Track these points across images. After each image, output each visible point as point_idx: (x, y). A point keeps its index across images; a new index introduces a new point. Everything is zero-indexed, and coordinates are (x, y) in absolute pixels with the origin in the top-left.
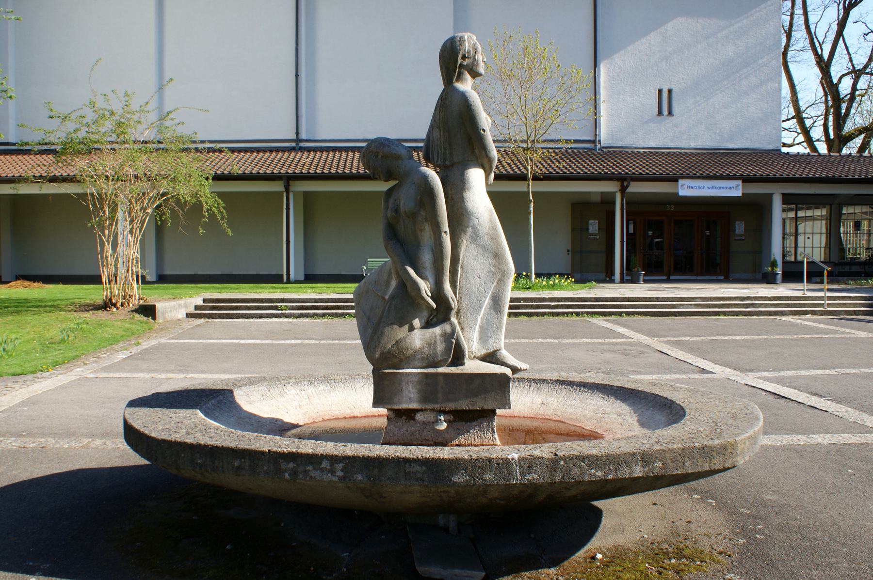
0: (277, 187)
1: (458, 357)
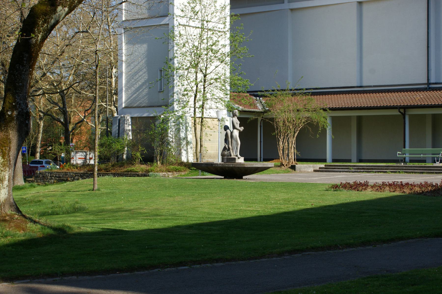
0: (396, 112)
1: (231, 156)
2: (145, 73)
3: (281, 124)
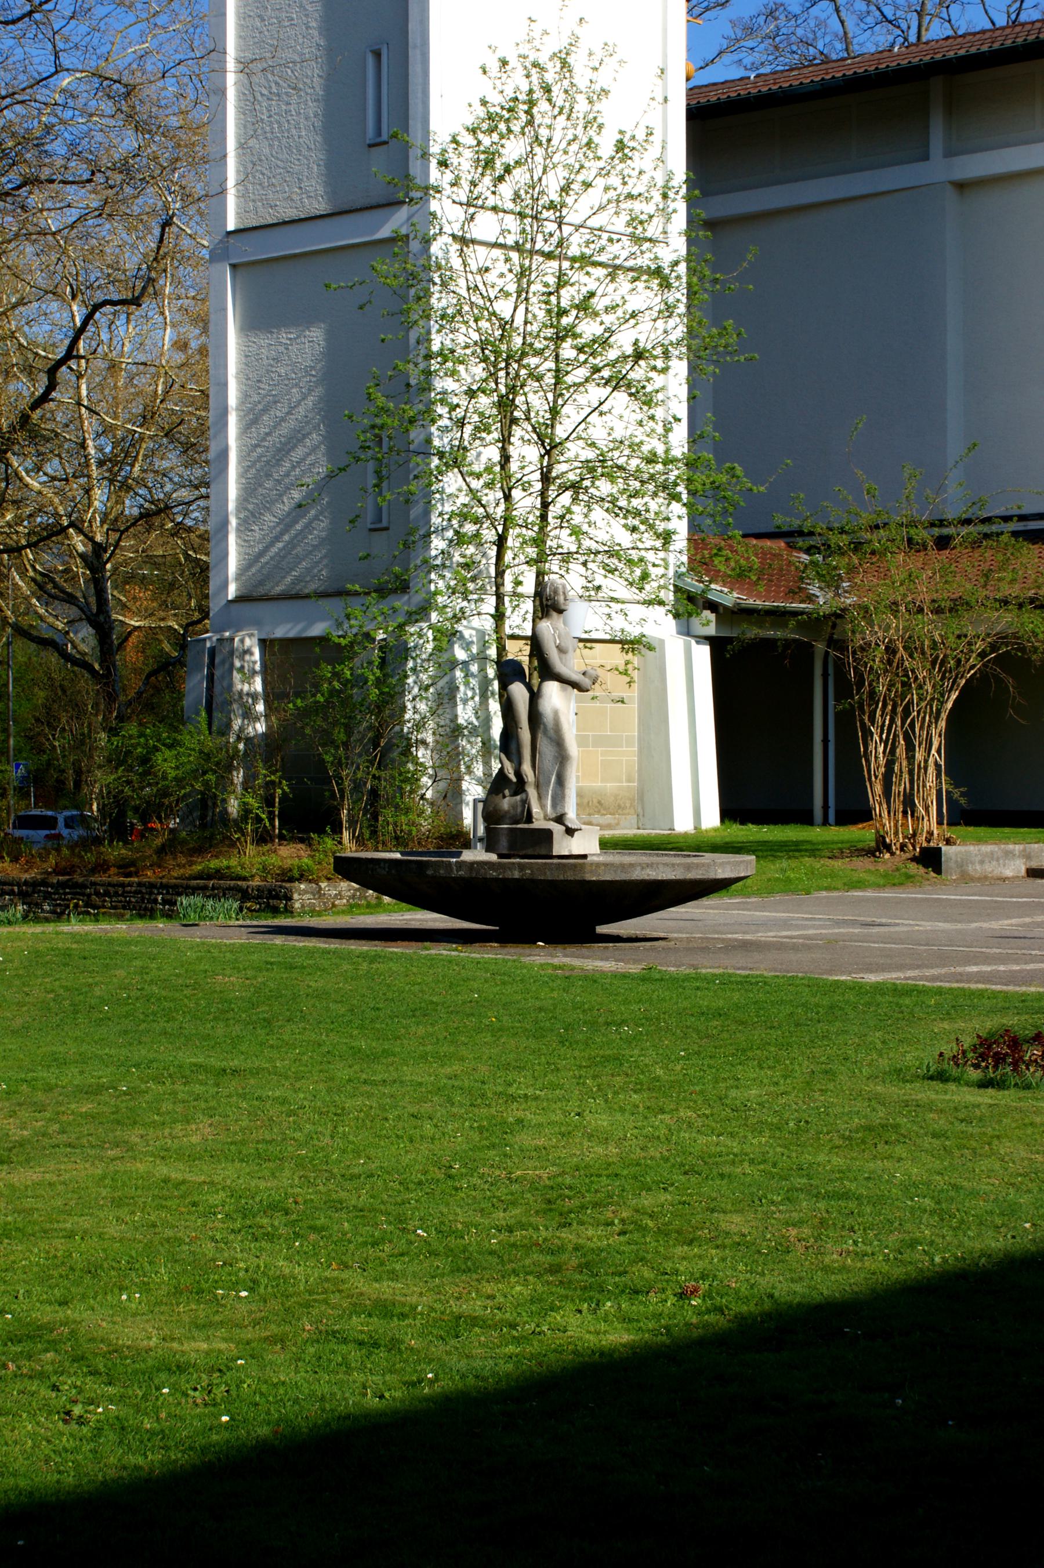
1: (529, 819)
2: (314, 449)
3: (877, 658)
